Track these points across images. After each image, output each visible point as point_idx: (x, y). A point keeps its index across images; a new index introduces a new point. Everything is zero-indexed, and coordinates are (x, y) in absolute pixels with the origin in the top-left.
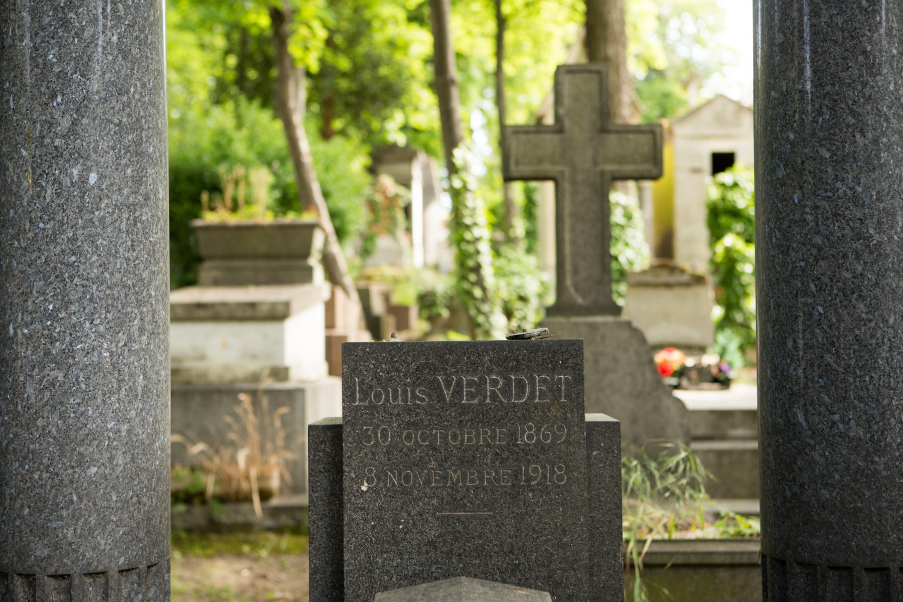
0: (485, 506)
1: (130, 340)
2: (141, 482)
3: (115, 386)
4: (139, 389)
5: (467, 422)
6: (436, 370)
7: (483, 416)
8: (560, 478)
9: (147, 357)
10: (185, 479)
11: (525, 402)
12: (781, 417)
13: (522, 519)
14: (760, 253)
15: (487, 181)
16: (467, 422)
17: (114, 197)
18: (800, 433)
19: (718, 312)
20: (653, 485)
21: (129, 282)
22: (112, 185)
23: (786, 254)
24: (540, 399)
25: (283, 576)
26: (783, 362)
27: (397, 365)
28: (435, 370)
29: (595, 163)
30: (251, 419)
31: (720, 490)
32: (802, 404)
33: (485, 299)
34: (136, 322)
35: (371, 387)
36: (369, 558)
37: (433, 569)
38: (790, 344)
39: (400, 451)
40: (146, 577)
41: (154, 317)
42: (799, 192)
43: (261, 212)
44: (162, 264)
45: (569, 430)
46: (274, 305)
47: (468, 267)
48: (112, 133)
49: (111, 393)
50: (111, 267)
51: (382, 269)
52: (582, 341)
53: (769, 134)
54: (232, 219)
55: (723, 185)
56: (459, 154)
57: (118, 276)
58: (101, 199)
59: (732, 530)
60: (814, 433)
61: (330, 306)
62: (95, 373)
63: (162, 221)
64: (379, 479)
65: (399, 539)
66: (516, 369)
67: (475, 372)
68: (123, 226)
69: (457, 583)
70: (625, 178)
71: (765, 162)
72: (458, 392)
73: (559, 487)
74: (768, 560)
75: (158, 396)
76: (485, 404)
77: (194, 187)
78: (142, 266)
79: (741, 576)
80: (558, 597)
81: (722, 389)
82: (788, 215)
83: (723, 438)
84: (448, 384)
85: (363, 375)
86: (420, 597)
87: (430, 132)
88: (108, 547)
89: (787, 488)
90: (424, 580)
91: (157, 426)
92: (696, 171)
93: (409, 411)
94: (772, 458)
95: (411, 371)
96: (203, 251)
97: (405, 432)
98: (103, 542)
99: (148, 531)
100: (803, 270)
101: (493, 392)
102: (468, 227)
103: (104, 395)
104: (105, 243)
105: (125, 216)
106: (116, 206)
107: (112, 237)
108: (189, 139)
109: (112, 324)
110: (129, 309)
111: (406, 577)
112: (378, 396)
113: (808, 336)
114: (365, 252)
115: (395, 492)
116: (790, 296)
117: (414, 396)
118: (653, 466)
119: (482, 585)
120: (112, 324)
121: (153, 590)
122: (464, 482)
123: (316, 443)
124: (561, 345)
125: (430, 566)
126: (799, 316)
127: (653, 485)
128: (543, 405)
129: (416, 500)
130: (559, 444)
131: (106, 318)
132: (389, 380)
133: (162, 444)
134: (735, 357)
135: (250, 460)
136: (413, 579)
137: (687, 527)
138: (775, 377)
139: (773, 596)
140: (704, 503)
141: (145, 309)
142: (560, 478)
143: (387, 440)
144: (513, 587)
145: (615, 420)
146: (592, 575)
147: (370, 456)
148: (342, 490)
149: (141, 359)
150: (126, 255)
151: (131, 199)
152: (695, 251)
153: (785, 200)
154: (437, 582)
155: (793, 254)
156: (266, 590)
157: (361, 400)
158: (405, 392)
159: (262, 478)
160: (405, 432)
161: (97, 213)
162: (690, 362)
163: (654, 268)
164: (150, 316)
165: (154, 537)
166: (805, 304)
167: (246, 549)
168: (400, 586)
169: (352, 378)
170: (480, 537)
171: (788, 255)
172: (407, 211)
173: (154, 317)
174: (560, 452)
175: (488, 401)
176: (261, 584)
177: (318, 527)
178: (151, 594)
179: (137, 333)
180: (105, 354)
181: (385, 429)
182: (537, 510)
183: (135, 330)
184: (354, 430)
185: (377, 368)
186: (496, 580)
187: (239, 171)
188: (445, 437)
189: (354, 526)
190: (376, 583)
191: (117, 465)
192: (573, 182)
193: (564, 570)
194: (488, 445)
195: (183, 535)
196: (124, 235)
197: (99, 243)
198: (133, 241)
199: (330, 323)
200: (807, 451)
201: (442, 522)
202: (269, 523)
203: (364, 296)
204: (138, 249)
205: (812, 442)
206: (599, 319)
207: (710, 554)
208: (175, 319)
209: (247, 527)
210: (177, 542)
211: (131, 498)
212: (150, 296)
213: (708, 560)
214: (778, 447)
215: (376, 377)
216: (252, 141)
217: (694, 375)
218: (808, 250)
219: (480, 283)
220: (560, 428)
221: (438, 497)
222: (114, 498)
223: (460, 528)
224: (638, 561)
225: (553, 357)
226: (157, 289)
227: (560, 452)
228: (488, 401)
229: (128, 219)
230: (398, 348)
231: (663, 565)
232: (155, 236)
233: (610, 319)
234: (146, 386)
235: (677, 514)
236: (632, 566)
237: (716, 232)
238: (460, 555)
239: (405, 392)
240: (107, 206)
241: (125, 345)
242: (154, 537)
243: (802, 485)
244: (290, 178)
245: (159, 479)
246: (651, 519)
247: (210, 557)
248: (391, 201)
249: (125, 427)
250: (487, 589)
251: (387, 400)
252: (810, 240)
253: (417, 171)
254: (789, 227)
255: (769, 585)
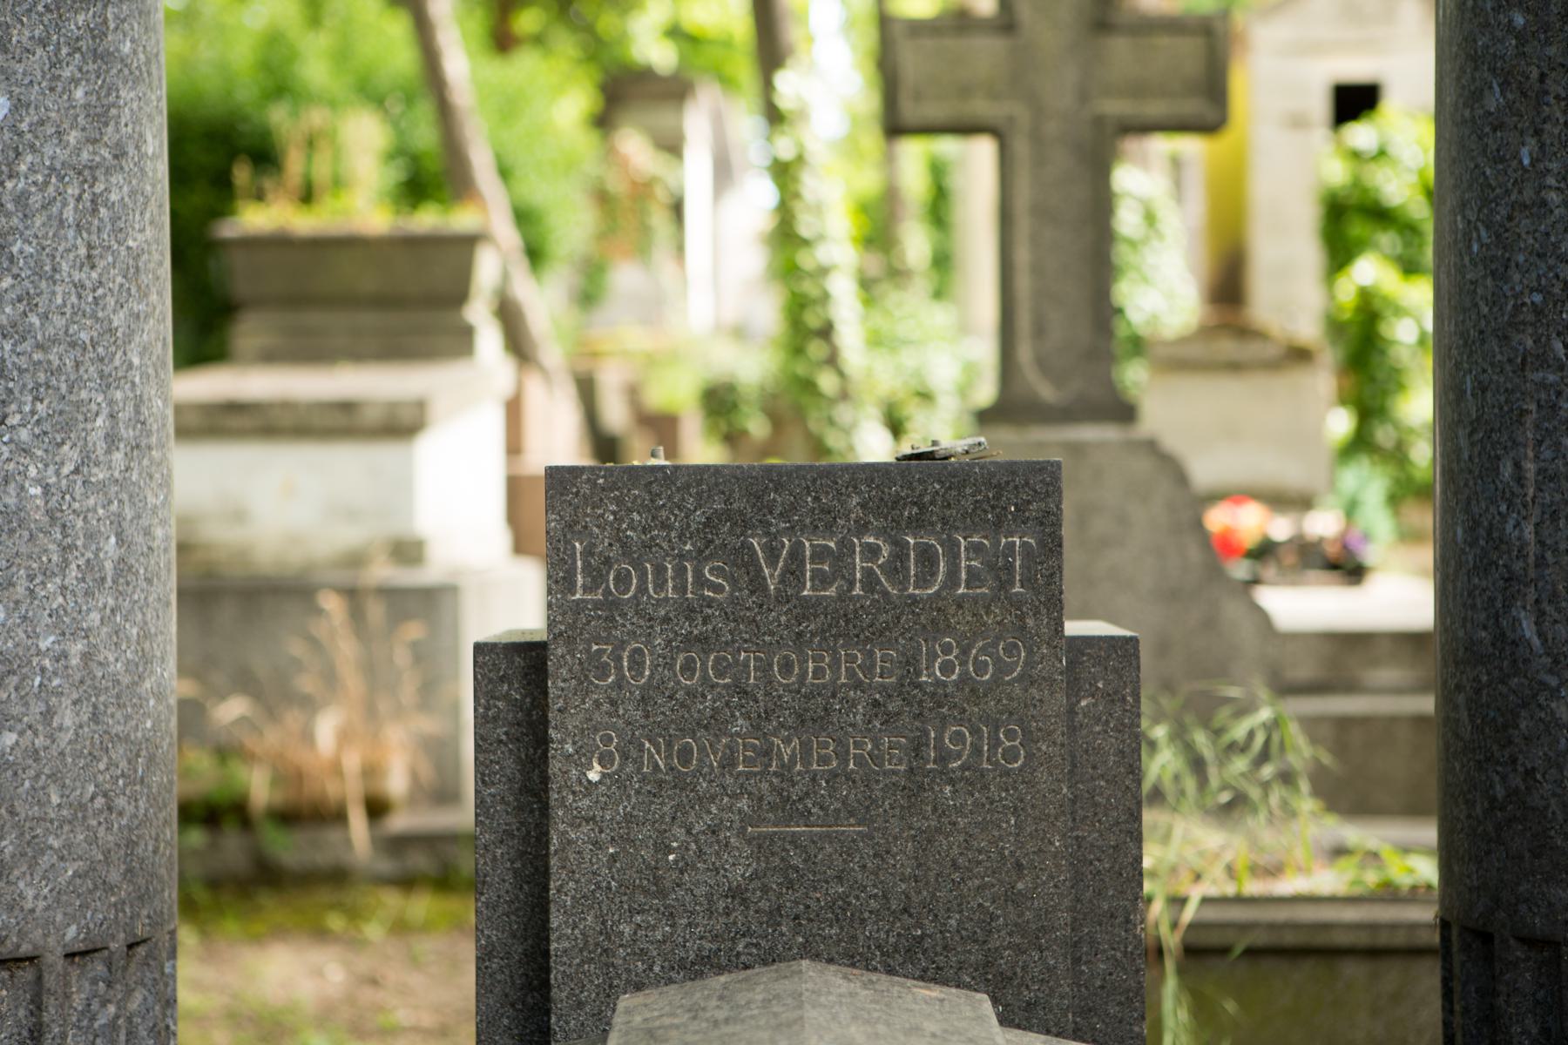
0: (851, 814)
1: (87, 459)
2: (112, 764)
3: (55, 558)
4: (108, 565)
5: (813, 635)
6: (746, 525)
7: (847, 622)
8: (1011, 755)
9: (125, 497)
10: (202, 773)
11: (937, 593)
12: (1485, 628)
13: (929, 841)
14: (1443, 276)
15: (848, 147)
16: (813, 635)
17: (48, 150)
18: (1526, 661)
19: (1341, 424)
20: (1203, 781)
21: (84, 336)
22: (42, 123)
23: (1500, 275)
24: (967, 587)
25: (415, 980)
26: (1492, 509)
27: (664, 513)
28: (744, 524)
29: (1084, 96)
30: (346, 649)
31: (1349, 794)
32: (1532, 595)
33: (844, 395)
34: (99, 422)
35: (607, 562)
36: (604, 923)
37: (740, 948)
38: (1507, 470)
39: (671, 698)
40: (125, 968)
41: (137, 412)
42: (1532, 142)
43: (363, 205)
44: (154, 298)
45: (1030, 652)
46: (393, 406)
47: (807, 328)
48: (40, 8)
49: (47, 574)
50: (42, 302)
51: (623, 337)
52: (1058, 464)
53: (1468, 15)
54: (303, 222)
55: (1356, 155)
56: (788, 84)
57: (59, 321)
58: (18, 154)
59: (1372, 878)
60: (1556, 662)
61: (514, 410)
62: (12, 532)
63: (153, 206)
64: (625, 757)
65: (668, 884)
66: (917, 524)
67: (830, 528)
68: (69, 214)
69: (793, 972)
70: (1146, 128)
71: (1458, 79)
72: (793, 573)
73: (1007, 773)
74: (1455, 932)
75: (149, 581)
76: (851, 598)
77: (218, 153)
78: (111, 301)
79: (1392, 974)
80: (1006, 1006)
81: (1343, 584)
82: (1508, 192)
83: (1350, 687)
84: (773, 554)
85: (591, 534)
86: (714, 1003)
87: (727, 44)
88: (42, 904)
89: (1497, 779)
90: (721, 969)
91: (147, 645)
92: (1298, 122)
93: (689, 612)
94: (1464, 715)
95: (693, 526)
96: (241, 287)
97: (682, 656)
98: (30, 893)
99: (130, 870)
100: (1538, 311)
101: (868, 573)
102: (806, 243)
103: (31, 578)
104: (29, 249)
105: (73, 191)
106: (52, 169)
107: (45, 237)
108: (206, 53)
109: (47, 426)
110: (84, 394)
111: (683, 965)
112: (623, 580)
113: (1548, 454)
114: (588, 296)
115: (660, 783)
116: (1508, 368)
117: (700, 581)
118: (1200, 739)
119: (845, 977)
120: (47, 426)
121: (138, 996)
122: (806, 762)
123: (490, 680)
124: (1014, 473)
125: (733, 939)
126: (1528, 412)
127: (1203, 781)
128: (975, 599)
129: (704, 801)
130: (1009, 683)
131: (33, 412)
132: (647, 546)
133: (159, 685)
134: (1378, 521)
135: (344, 737)
136: (696, 968)
137: (1274, 871)
138: (1473, 544)
139: (1466, 1010)
140: (1314, 825)
141: (119, 395)
142: (1011, 755)
143: (642, 674)
144: (910, 982)
145: (1128, 633)
146: (1077, 961)
147: (606, 707)
148: (545, 779)
149: (110, 502)
150: (77, 276)
151: (85, 155)
152: (1294, 292)
153: (1502, 160)
154: (749, 972)
155: (1517, 277)
156: (380, 1009)
157: (586, 589)
158: (680, 572)
159: (371, 771)
160: (682, 656)
161: (9, 185)
162: (1281, 528)
163: (1206, 332)
164: (130, 408)
165: (141, 881)
166: (1542, 385)
167: (335, 922)
168: (671, 981)
169: (567, 542)
170: (840, 878)
171: (1505, 278)
172: (677, 209)
173: (137, 412)
174: (1011, 699)
175: (857, 591)
176: (367, 995)
177: (494, 859)
178: (134, 1005)
179: (101, 446)
180: (33, 491)
181: (638, 651)
182: (962, 822)
183: (97, 438)
184: (572, 653)
185: (622, 520)
186: (875, 969)
187: (316, 117)
188: (764, 668)
189: (572, 856)
190: (619, 976)
191: (60, 729)
192: (1036, 137)
193: (1019, 950)
194: (858, 685)
195: (201, 895)
196: (71, 233)
197: (15, 249)
198: (90, 247)
199: (514, 447)
200: (1541, 699)
201: (760, 847)
202: (386, 866)
203: (587, 390)
204: (102, 263)
205: (1553, 681)
206: (1089, 433)
207: (1326, 927)
208: (186, 432)
209: (338, 877)
210: (189, 908)
211: (92, 799)
212: (130, 366)
213: (1321, 940)
214: (1478, 691)
215: (619, 540)
216: (342, 56)
217: (1290, 559)
218: (1550, 268)
219: (832, 360)
220: (1011, 649)
221: (750, 794)
222: (55, 799)
223: (796, 861)
224: (1172, 941)
225: (998, 497)
226: (145, 351)
227: (1011, 699)
228: (857, 591)
229: (79, 199)
230: (666, 477)
231: (1224, 951)
232: (139, 236)
233: (1105, 433)
234: (122, 560)
235: (1254, 844)
236: (1160, 952)
237: (1339, 250)
238: (797, 917)
239: (680, 572)
240: (32, 169)
241: (77, 471)
242: (141, 881)
243: (1529, 773)
244: (425, 136)
245: (151, 759)
246: (1201, 854)
247: (258, 940)
248: (642, 190)
249: (77, 647)
250: (855, 986)
251: (642, 589)
252: (1556, 246)
253: (696, 123)
254: (1510, 218)
255: (1457, 986)
